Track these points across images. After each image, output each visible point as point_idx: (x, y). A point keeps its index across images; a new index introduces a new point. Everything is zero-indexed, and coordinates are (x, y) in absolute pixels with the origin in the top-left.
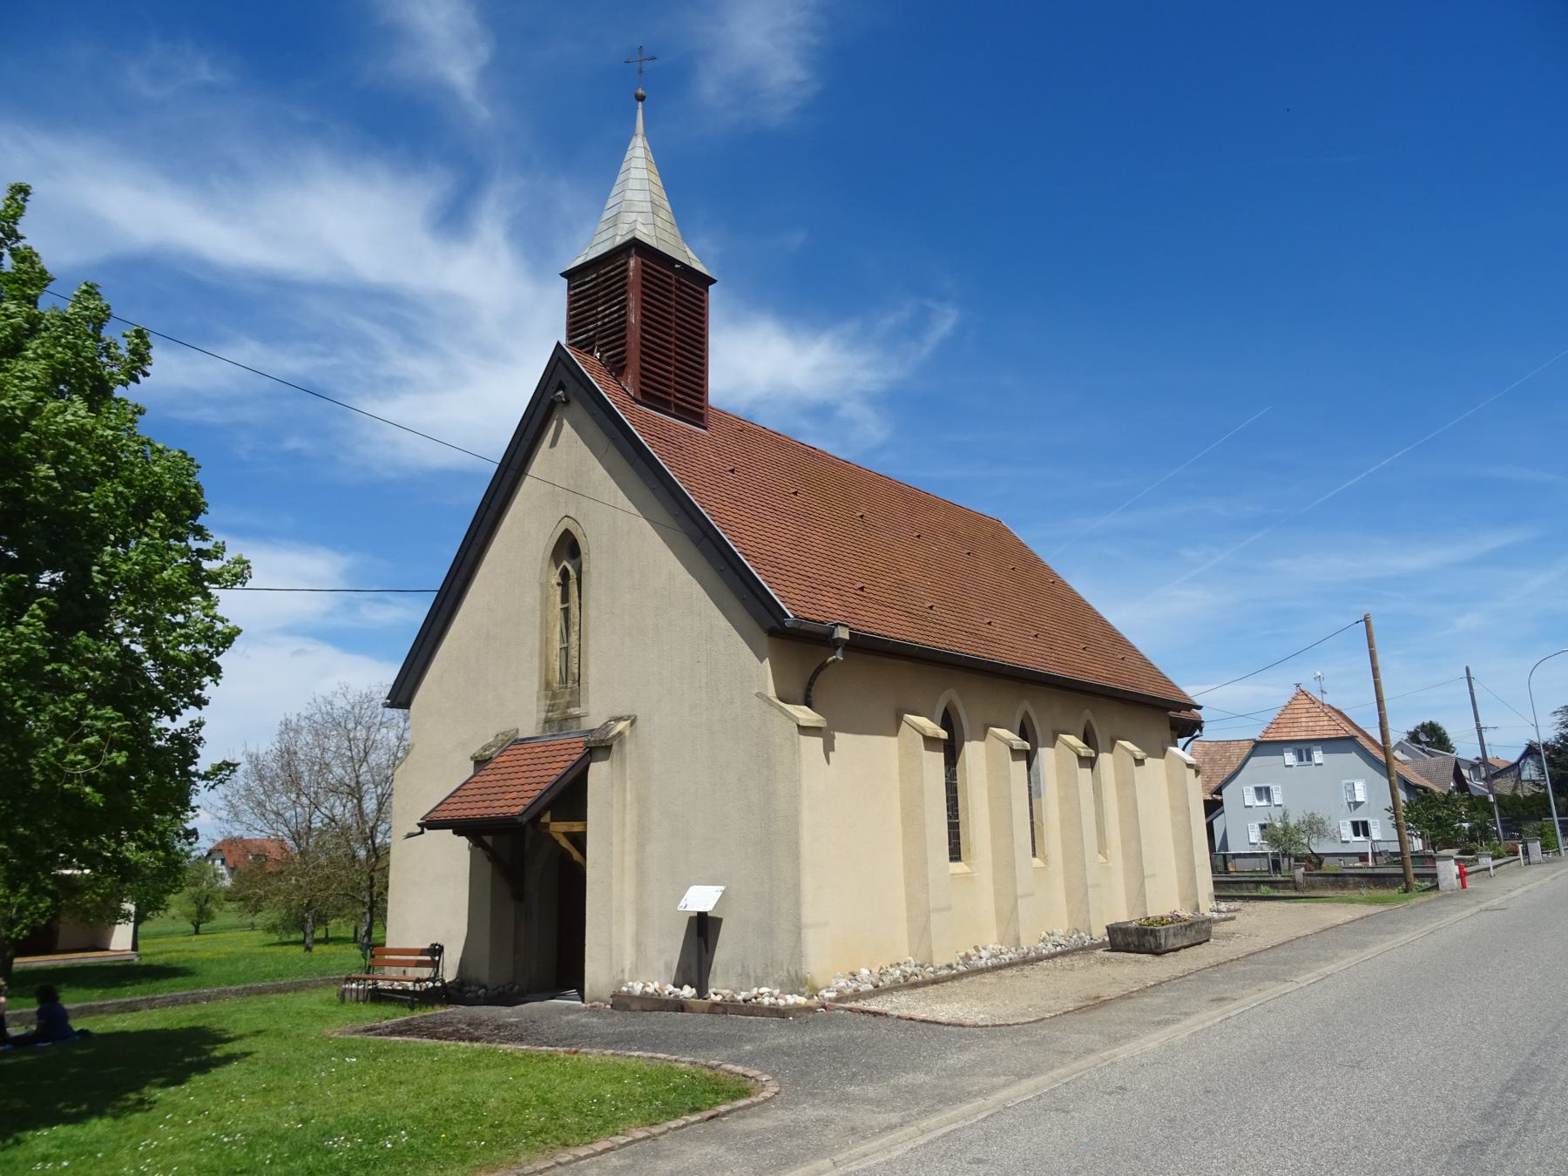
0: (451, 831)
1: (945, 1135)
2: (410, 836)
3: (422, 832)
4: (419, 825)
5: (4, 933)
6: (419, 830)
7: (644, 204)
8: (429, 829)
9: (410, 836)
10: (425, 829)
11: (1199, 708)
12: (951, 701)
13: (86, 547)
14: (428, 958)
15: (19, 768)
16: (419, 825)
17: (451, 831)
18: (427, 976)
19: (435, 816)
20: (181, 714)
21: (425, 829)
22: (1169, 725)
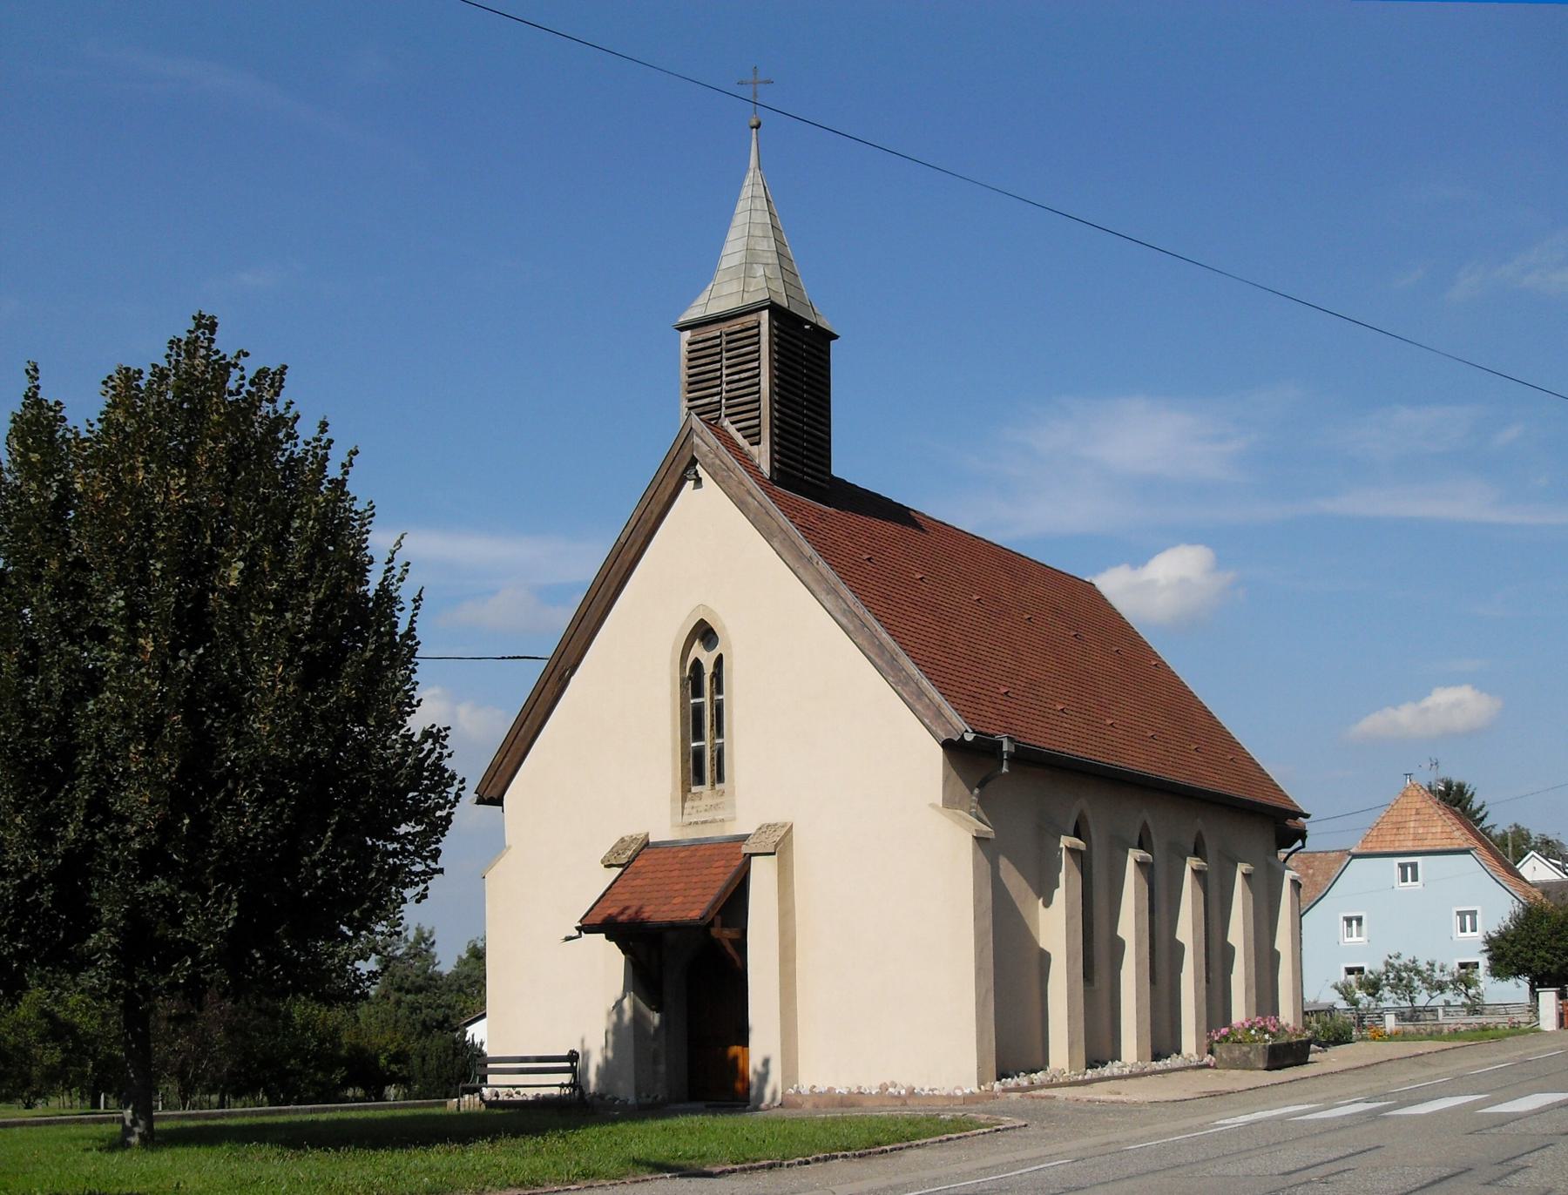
0: (604, 935)
1: (1021, 1174)
2: (568, 939)
3: (580, 936)
4: (577, 928)
5: (2, 1068)
6: (577, 933)
7: (769, 254)
8: (586, 933)
9: (568, 939)
10: (583, 933)
11: (1307, 816)
12: (1082, 811)
13: (28, 946)
14: (568, 1064)
15: (31, 440)
16: (577, 928)
17: (604, 935)
18: (566, 1082)
19: (587, 921)
20: (415, 622)
21: (583, 933)
22: (1274, 836)
